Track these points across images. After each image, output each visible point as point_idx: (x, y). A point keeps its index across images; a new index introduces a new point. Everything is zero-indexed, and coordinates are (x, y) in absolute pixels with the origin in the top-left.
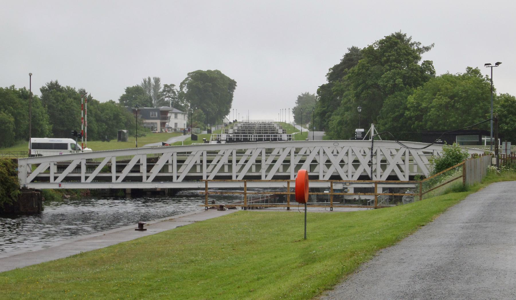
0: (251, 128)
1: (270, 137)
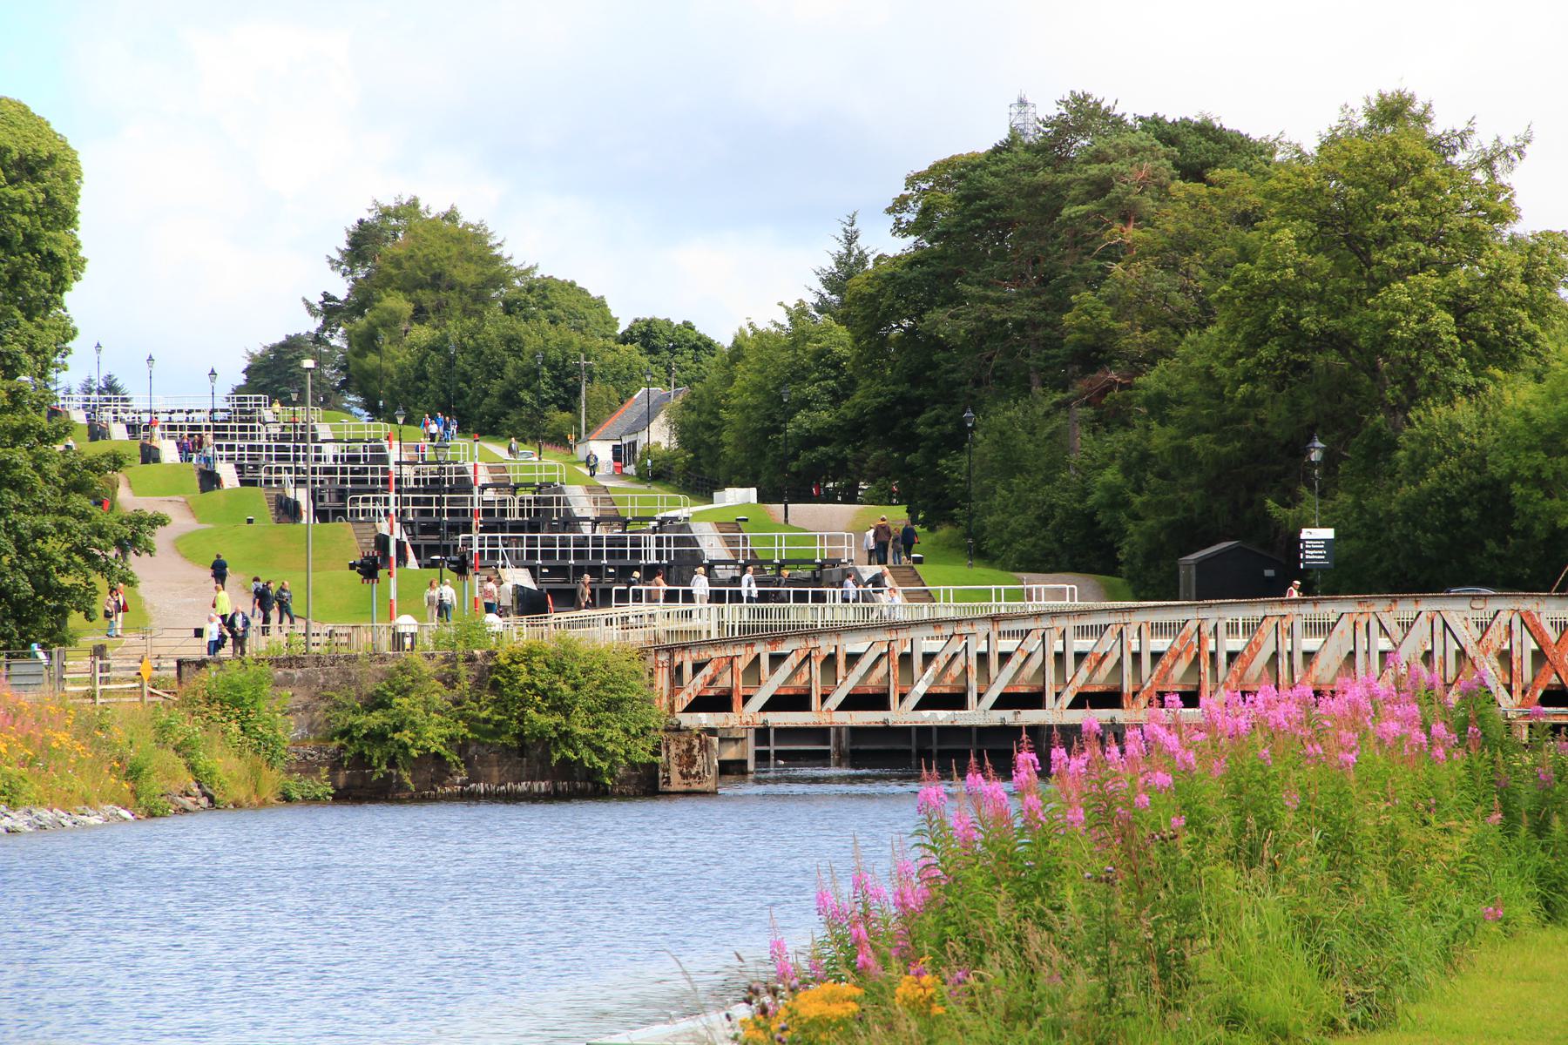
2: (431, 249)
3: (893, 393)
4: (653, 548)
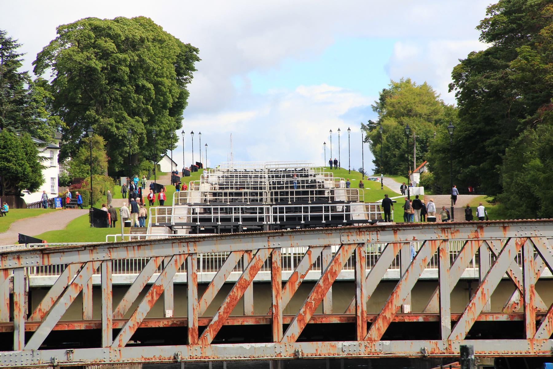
0: (307, 187)
1: (213, 215)
2: (407, 99)
3: (475, 129)
4: (271, 214)
